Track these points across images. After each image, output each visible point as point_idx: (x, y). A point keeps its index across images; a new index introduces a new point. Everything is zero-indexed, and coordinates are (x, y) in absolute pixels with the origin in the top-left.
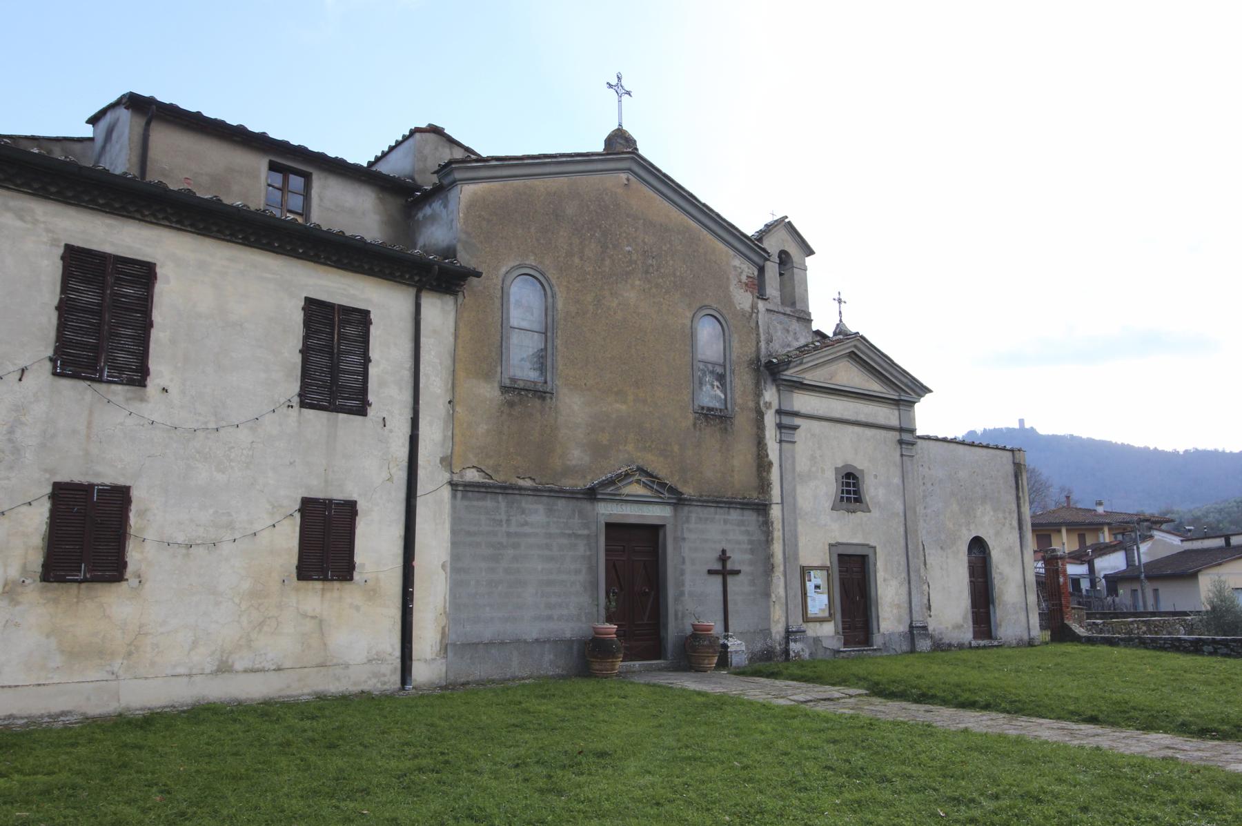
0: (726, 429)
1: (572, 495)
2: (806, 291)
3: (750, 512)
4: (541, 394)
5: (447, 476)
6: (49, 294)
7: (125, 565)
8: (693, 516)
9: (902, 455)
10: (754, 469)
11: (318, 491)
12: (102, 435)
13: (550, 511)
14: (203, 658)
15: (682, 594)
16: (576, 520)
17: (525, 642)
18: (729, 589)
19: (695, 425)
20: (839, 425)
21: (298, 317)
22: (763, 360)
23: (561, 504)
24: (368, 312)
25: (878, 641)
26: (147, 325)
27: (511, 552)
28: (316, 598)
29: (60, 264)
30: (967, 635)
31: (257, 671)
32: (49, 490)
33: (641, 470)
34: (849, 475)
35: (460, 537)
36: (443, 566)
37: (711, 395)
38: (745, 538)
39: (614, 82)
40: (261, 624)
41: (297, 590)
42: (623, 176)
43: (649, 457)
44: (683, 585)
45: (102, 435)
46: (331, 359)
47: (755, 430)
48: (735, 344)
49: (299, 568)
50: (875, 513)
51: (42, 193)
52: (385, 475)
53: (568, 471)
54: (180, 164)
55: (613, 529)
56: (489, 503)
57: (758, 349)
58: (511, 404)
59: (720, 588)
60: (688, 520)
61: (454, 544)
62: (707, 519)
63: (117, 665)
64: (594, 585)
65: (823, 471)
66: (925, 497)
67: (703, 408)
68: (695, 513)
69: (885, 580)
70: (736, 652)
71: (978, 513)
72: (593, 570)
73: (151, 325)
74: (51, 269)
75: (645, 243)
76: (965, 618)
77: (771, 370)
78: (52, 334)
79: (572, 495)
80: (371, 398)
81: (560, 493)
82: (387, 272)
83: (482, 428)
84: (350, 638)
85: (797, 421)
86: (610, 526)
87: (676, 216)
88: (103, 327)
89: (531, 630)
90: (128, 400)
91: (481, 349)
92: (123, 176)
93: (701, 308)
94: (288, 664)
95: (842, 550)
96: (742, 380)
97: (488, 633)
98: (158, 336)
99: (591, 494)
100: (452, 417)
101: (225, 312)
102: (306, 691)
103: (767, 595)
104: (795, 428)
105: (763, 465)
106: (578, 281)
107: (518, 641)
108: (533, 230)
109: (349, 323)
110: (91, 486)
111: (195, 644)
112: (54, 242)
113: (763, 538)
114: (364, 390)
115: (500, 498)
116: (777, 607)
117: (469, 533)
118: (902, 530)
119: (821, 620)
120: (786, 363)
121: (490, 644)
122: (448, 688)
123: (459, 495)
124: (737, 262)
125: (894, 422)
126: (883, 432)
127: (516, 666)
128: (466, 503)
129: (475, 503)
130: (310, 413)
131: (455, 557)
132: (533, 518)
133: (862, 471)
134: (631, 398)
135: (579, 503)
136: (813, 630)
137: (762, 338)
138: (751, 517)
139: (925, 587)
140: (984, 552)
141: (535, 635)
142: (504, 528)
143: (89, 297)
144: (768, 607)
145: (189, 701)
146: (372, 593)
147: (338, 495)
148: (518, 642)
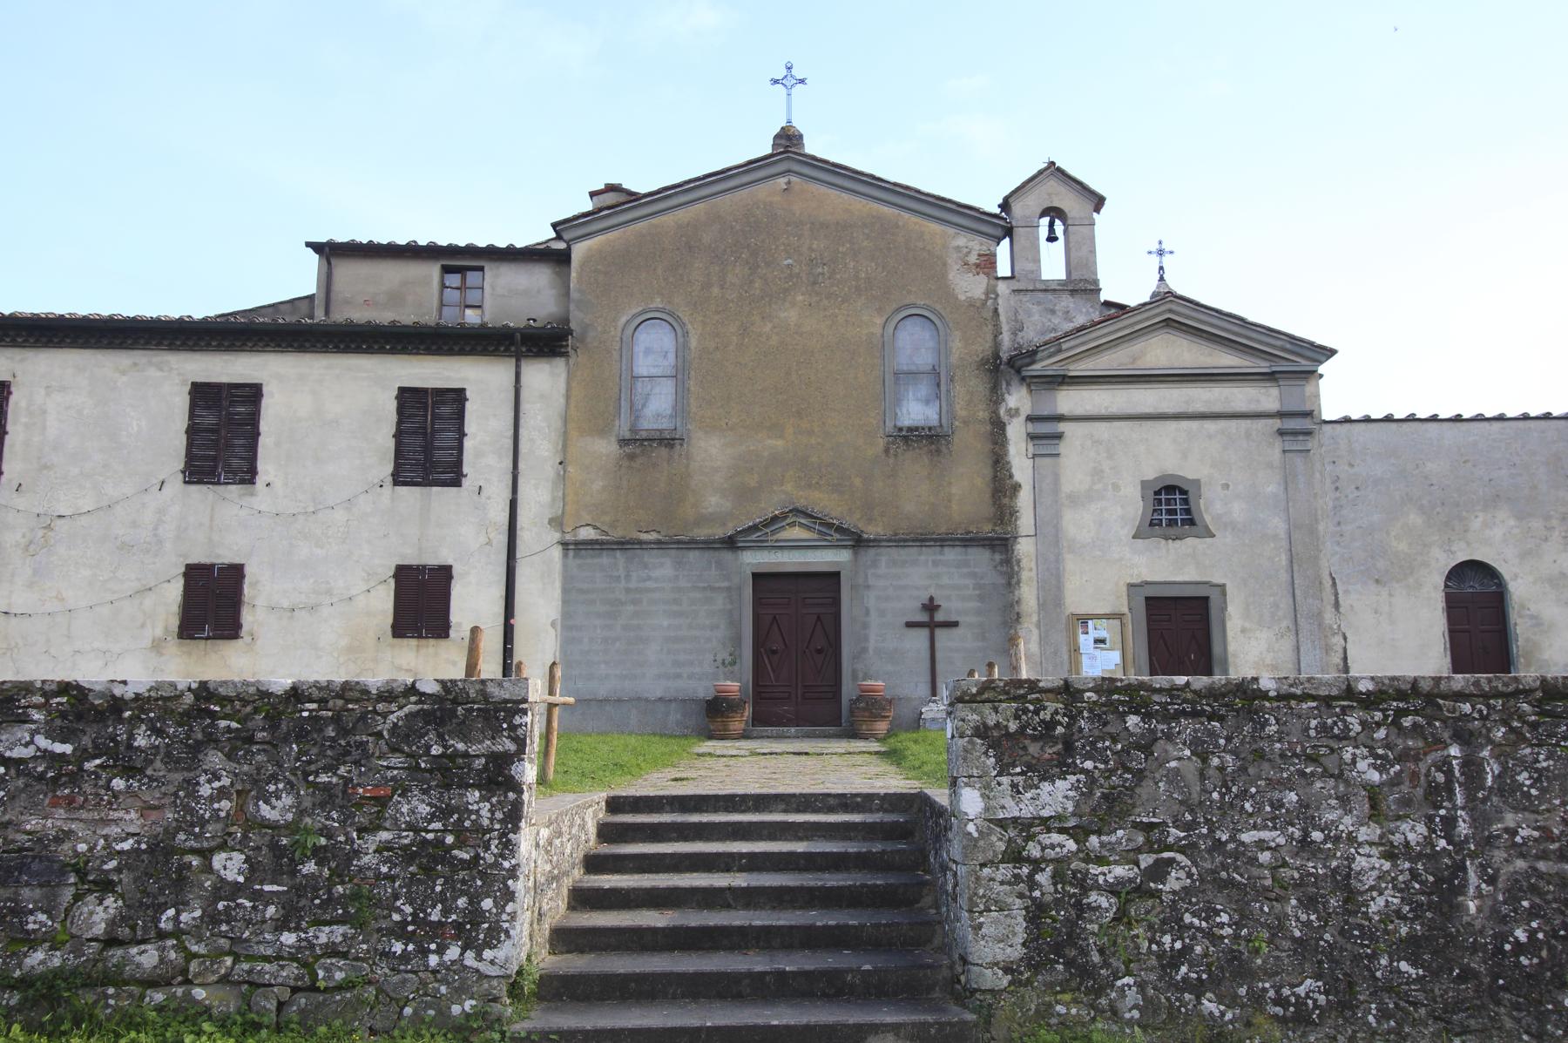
0: (938, 451)
1: (708, 545)
2: (1093, 252)
3: (981, 550)
4: (668, 441)
5: (557, 536)
6: (181, 422)
7: (240, 626)
8: (884, 559)
10: (987, 496)
11: (412, 559)
12: (222, 525)
15: (865, 650)
17: (647, 700)
18: (938, 645)
19: (887, 451)
20: (1149, 423)
21: (392, 405)
22: (1005, 356)
23: (693, 555)
24: (463, 390)
26: (255, 435)
27: (630, 608)
29: (188, 398)
33: (797, 511)
34: (1170, 489)
37: (916, 411)
38: (969, 582)
39: (798, 73)
41: (392, 646)
42: (782, 181)
43: (816, 495)
45: (222, 525)
49: (393, 627)
52: (483, 539)
53: (701, 520)
55: (760, 579)
56: (605, 559)
57: (997, 345)
58: (632, 457)
59: (926, 644)
60: (875, 564)
61: (565, 602)
64: (737, 640)
65: (1116, 487)
66: (1337, 508)
67: (901, 429)
68: (885, 558)
69: (1243, 631)
71: (1476, 524)
72: (735, 624)
73: (259, 434)
74: (181, 402)
77: (1009, 367)
78: (183, 453)
79: (708, 545)
80: (465, 470)
81: (692, 544)
82: (456, 348)
83: (598, 485)
86: (756, 576)
87: (861, 206)
88: (222, 439)
89: (656, 690)
90: (240, 496)
93: (898, 310)
95: (1153, 592)
96: (969, 391)
97: (602, 692)
98: (266, 442)
99: (730, 543)
100: (562, 478)
101: (330, 413)
104: (1059, 436)
105: (1002, 488)
107: (639, 699)
108: (659, 271)
109: (443, 403)
110: (213, 565)
112: (183, 382)
113: (1002, 581)
114: (458, 463)
115: (618, 553)
117: (581, 591)
120: (1032, 355)
121: (606, 700)
123: (571, 553)
124: (962, 240)
126: (1244, 424)
128: (579, 561)
129: (589, 561)
131: (566, 615)
132: (657, 573)
133: (1197, 483)
135: (717, 553)
137: (1005, 328)
138: (981, 559)
141: (659, 694)
143: (209, 420)
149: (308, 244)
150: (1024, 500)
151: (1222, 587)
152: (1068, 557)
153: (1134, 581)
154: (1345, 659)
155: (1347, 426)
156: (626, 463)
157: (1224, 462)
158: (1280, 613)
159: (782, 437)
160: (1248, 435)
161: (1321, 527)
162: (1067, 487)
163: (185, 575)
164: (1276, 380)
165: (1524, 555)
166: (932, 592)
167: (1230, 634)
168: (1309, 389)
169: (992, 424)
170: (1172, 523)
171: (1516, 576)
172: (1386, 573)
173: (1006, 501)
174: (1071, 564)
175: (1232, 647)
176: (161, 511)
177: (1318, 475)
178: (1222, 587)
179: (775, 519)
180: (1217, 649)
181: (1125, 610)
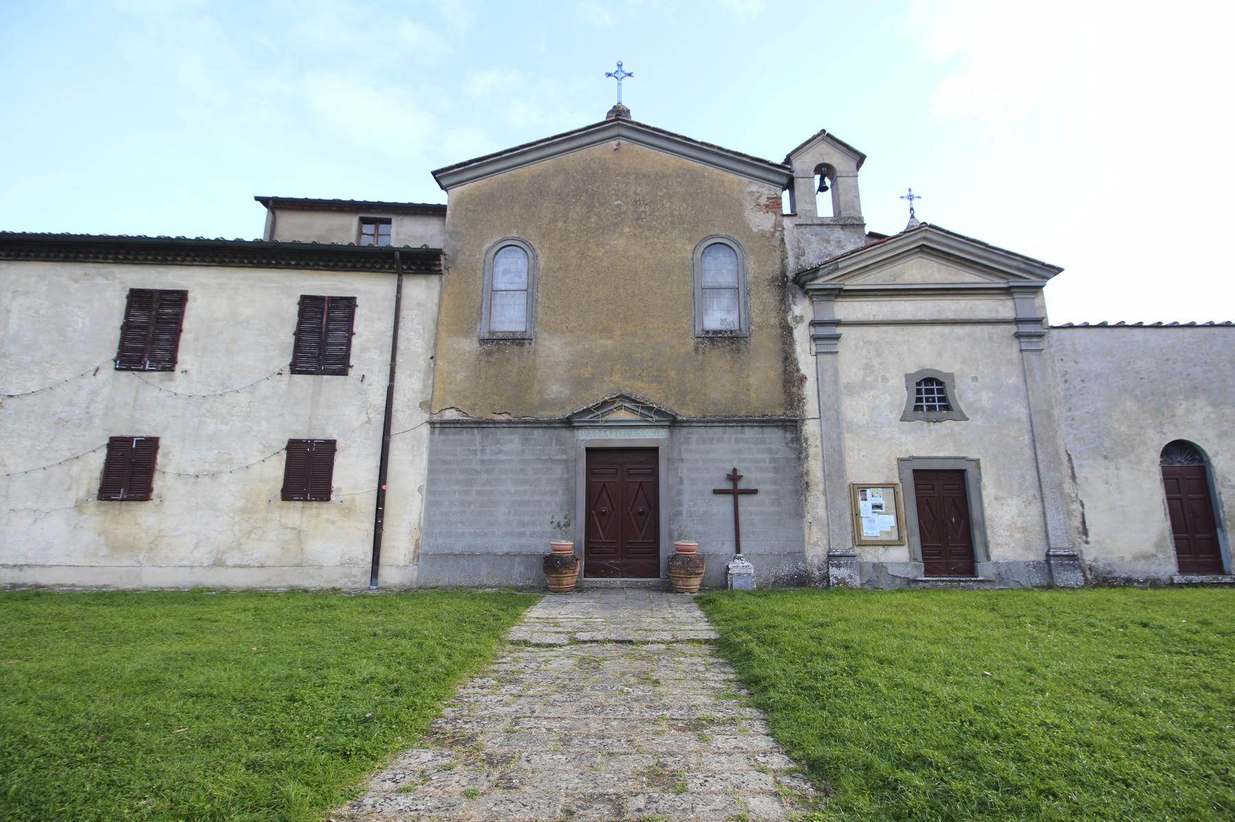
0: (739, 350)
1: (550, 425)
3: (775, 429)
5: (427, 416)
9: (1021, 351)
13: (526, 440)
14: (203, 555)
15: (679, 513)
16: (554, 447)
17: (495, 555)
18: (740, 509)
19: (696, 349)
20: (910, 328)
23: (537, 433)
25: (985, 570)
27: (484, 477)
28: (297, 514)
29: (125, 301)
30: (1167, 566)
31: (244, 566)
32: (107, 441)
33: (623, 397)
34: (929, 381)
35: (437, 467)
36: (420, 490)
37: (718, 316)
38: (766, 456)
40: (250, 533)
41: (281, 508)
42: (613, 144)
43: (639, 384)
44: (680, 504)
45: (144, 404)
46: (320, 336)
47: (780, 346)
48: (751, 265)
50: (976, 421)
51: (117, 261)
52: (363, 418)
53: (545, 404)
54: (296, 229)
55: (593, 453)
56: (465, 436)
57: (784, 267)
58: (489, 353)
60: (687, 441)
61: (430, 471)
62: (712, 439)
63: (142, 556)
65: (885, 379)
66: (1068, 397)
67: (708, 332)
69: (997, 498)
70: (739, 575)
71: (1181, 410)
72: (570, 491)
73: (181, 331)
74: (120, 304)
75: (636, 194)
76: (1159, 545)
78: (117, 345)
79: (550, 425)
80: (352, 362)
81: (537, 424)
83: (462, 375)
84: (328, 544)
85: (839, 330)
86: (589, 451)
87: (674, 162)
88: (150, 336)
90: (161, 381)
91: (465, 312)
92: (257, 242)
93: (705, 239)
94: (270, 563)
97: (459, 547)
98: (186, 338)
99: (568, 423)
100: (433, 370)
102: (283, 584)
103: (799, 515)
104: (837, 338)
105: (791, 379)
106: (561, 241)
107: (488, 554)
108: (516, 210)
109: (337, 308)
111: (197, 545)
113: (793, 456)
116: (815, 529)
117: (445, 462)
118: (1027, 438)
119: (886, 545)
121: (461, 555)
122: (406, 593)
123: (437, 431)
124: (755, 187)
125: (1010, 314)
127: (485, 574)
128: (443, 437)
130: (299, 378)
131: (431, 482)
132: (508, 447)
133: (951, 375)
134: (618, 333)
136: (869, 556)
137: (790, 253)
138: (775, 437)
139: (1076, 507)
140: (1201, 460)
141: (506, 549)
142: (479, 456)
143: (141, 318)
144: (802, 529)
145: (190, 585)
146: (348, 510)
147: (319, 436)
148: (488, 555)
149: (257, 199)
150: (809, 389)
151: (977, 461)
152: (847, 436)
153: (903, 456)
154: (1084, 522)
155: (1070, 331)
156: (484, 358)
157: (973, 358)
158: (1027, 484)
159: (611, 338)
160: (991, 338)
161: (1056, 412)
162: (844, 379)
163: (287, 448)
164: (1011, 294)
165: (1222, 435)
166: (735, 464)
167: (986, 501)
168: (1037, 301)
169: (782, 327)
170: (931, 408)
171: (1216, 454)
172: (1112, 451)
173: (794, 390)
174: (849, 442)
175: (988, 512)
176: (94, 393)
177: (1049, 370)
178: (977, 461)
179: (605, 403)
180: (975, 513)
181: (897, 480)
